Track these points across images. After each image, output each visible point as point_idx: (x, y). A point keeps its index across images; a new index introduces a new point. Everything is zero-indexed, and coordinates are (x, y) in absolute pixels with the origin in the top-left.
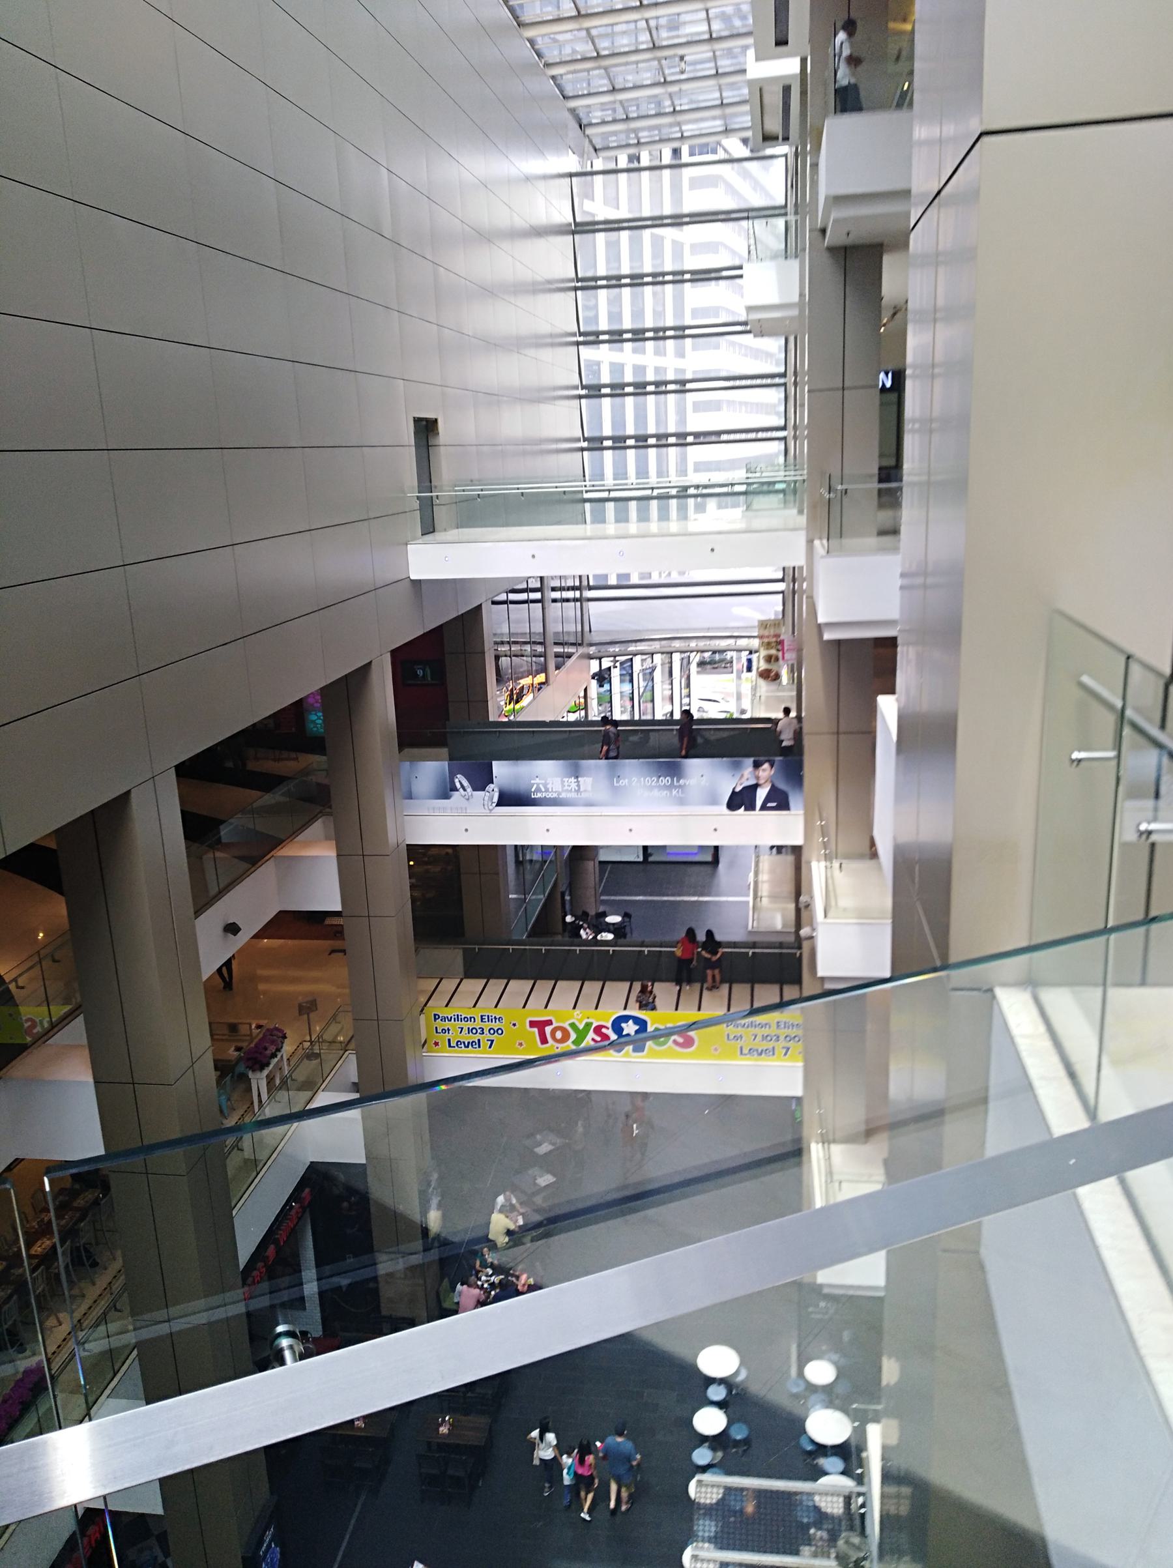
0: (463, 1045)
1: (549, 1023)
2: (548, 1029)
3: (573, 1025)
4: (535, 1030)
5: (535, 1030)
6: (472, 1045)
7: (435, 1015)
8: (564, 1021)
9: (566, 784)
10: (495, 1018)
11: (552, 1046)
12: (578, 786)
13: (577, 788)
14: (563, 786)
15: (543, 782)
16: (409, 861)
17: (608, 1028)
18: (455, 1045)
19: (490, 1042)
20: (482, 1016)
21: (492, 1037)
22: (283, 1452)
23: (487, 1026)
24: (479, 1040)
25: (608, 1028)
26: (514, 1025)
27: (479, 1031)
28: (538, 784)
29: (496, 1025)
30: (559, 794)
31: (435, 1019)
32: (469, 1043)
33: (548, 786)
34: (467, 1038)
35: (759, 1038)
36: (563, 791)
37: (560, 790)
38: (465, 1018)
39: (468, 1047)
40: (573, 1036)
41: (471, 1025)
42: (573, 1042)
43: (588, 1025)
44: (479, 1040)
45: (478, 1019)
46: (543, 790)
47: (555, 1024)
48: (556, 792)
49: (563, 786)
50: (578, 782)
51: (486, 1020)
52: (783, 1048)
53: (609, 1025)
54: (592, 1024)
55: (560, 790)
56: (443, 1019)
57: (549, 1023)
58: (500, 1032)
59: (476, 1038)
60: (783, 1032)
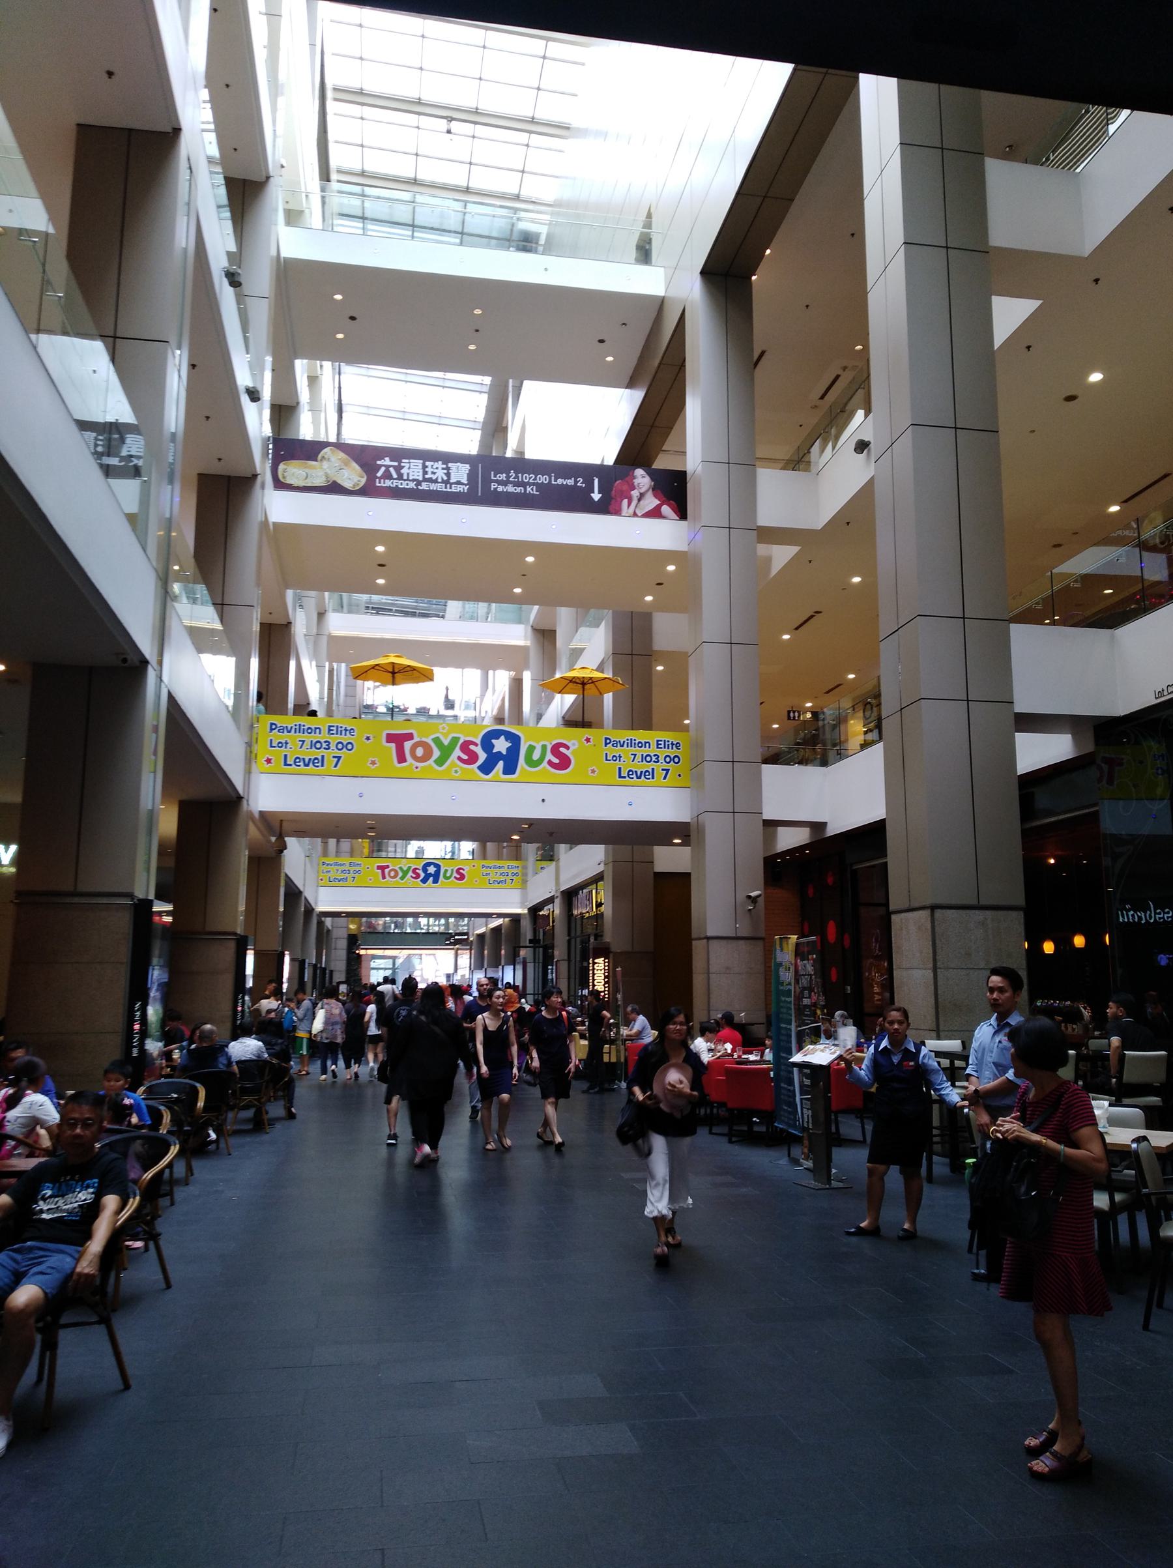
0: (634, 776)
1: (410, 737)
2: (408, 745)
3: (401, 868)
4: (393, 745)
5: (393, 745)
6: (314, 763)
7: (606, 739)
8: (427, 737)
9: (429, 470)
10: (672, 744)
11: (411, 765)
12: (448, 475)
13: (445, 478)
14: (425, 473)
15: (396, 464)
16: (870, 587)
17: (476, 745)
18: (626, 775)
19: (665, 772)
20: (658, 741)
21: (338, 753)
22: (935, 1268)
23: (334, 739)
24: (323, 756)
25: (476, 745)
26: (368, 738)
27: (654, 759)
28: (387, 467)
29: (346, 739)
30: (419, 483)
31: (606, 744)
32: (642, 772)
33: (402, 471)
34: (309, 753)
35: (307, 745)
36: (425, 480)
37: (421, 478)
38: (639, 743)
39: (640, 778)
40: (436, 753)
41: (315, 737)
42: (435, 761)
43: (455, 740)
44: (323, 756)
45: (653, 745)
46: (395, 476)
47: (416, 739)
48: (413, 480)
49: (425, 473)
50: (448, 469)
51: (662, 746)
52: (334, 757)
53: (478, 741)
54: (459, 738)
55: (421, 478)
56: (282, 730)
57: (410, 737)
58: (350, 747)
59: (318, 754)
60: (662, 753)
